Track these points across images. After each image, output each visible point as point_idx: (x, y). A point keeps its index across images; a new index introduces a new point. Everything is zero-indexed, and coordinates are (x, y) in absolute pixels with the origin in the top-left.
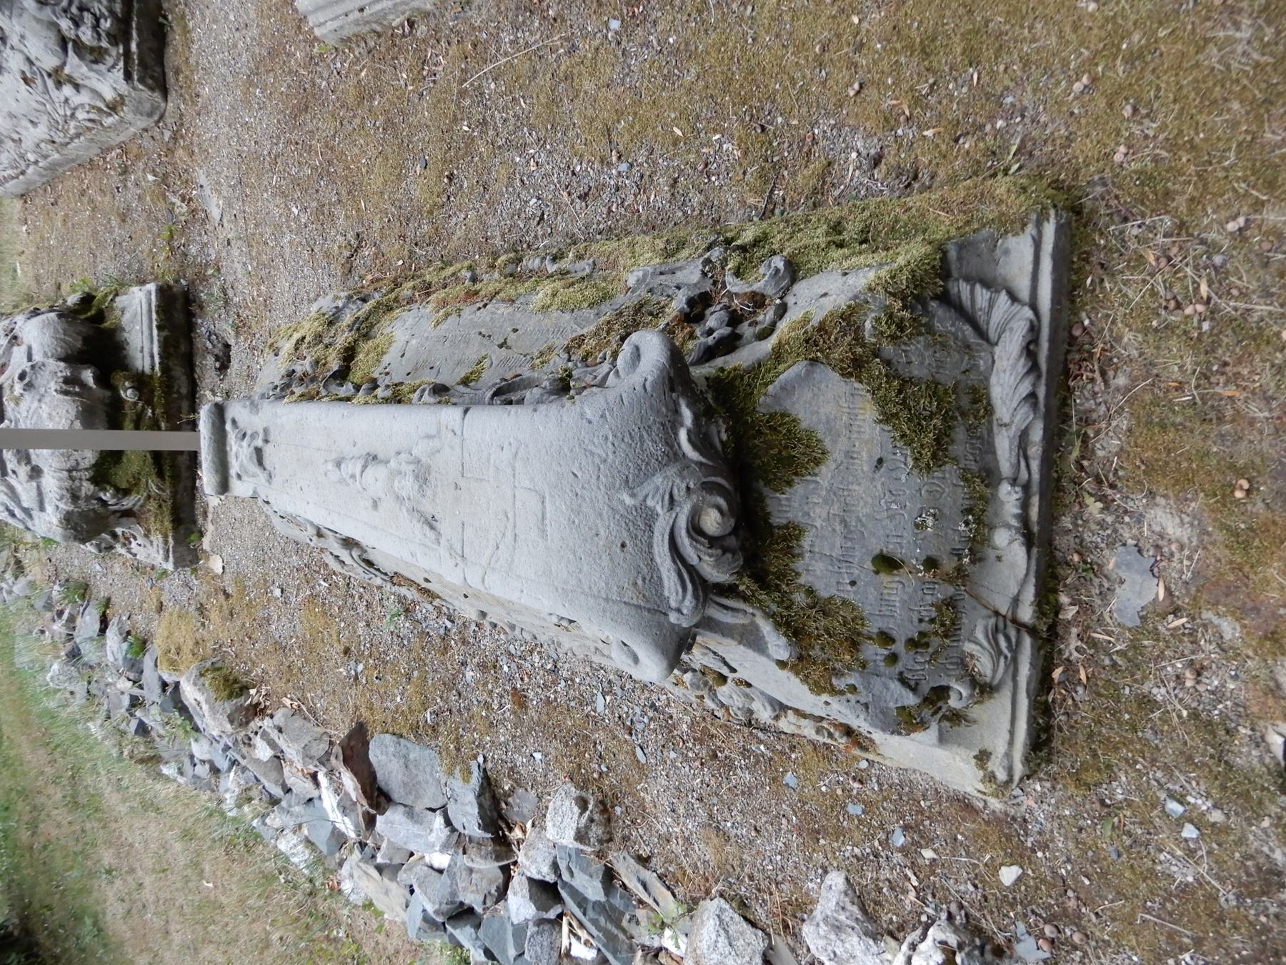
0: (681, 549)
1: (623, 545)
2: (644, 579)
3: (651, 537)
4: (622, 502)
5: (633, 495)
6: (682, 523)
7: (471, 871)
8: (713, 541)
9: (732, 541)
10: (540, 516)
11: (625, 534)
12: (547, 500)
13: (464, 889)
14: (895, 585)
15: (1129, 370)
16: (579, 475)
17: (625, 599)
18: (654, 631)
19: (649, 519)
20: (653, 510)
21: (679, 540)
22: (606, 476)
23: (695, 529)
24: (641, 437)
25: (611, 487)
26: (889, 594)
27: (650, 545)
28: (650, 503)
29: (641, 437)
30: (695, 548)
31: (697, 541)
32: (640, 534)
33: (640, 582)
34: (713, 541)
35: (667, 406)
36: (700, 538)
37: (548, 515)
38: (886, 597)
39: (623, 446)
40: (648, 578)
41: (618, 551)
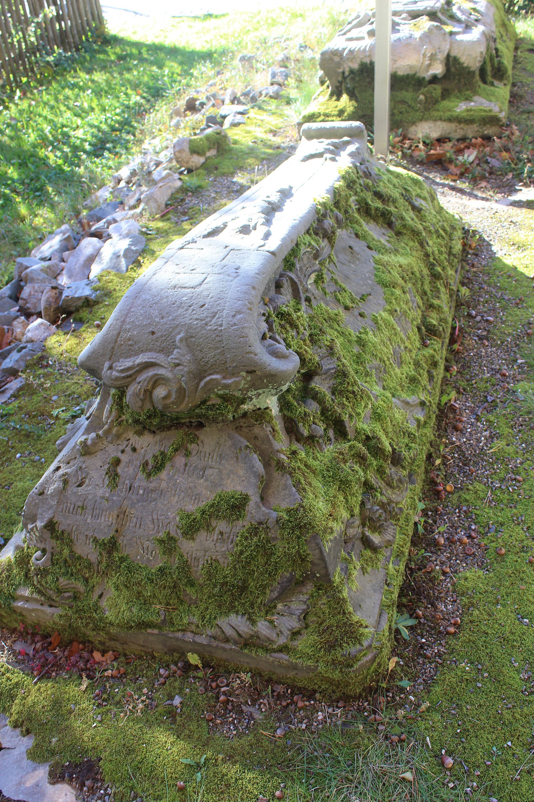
0: (146, 371)
1: (153, 333)
2: (131, 345)
3: (155, 351)
4: (179, 333)
5: (181, 340)
6: (161, 371)
7: (42, 292)
8: (149, 393)
9: (148, 406)
10: (184, 286)
11: (160, 334)
12: (193, 290)
13: (34, 287)
14: (110, 519)
15: (24, 376)
16: (202, 309)
17: (122, 333)
18: (101, 351)
19: (166, 351)
20: (172, 353)
21: (151, 369)
22: (197, 324)
23: (157, 381)
24: (218, 348)
25: (190, 327)
26: (105, 516)
27: (150, 350)
28: (175, 351)
29: (218, 348)
30: (145, 380)
31: (148, 383)
32: (158, 344)
33: (130, 342)
34: (149, 393)
35: (236, 367)
36: (151, 383)
37: (183, 290)
38: (104, 514)
39: (214, 336)
40: (132, 348)
41: (151, 329)
